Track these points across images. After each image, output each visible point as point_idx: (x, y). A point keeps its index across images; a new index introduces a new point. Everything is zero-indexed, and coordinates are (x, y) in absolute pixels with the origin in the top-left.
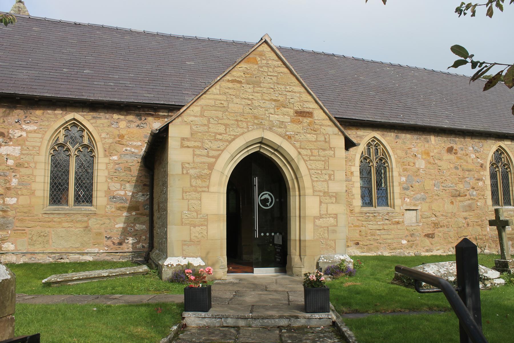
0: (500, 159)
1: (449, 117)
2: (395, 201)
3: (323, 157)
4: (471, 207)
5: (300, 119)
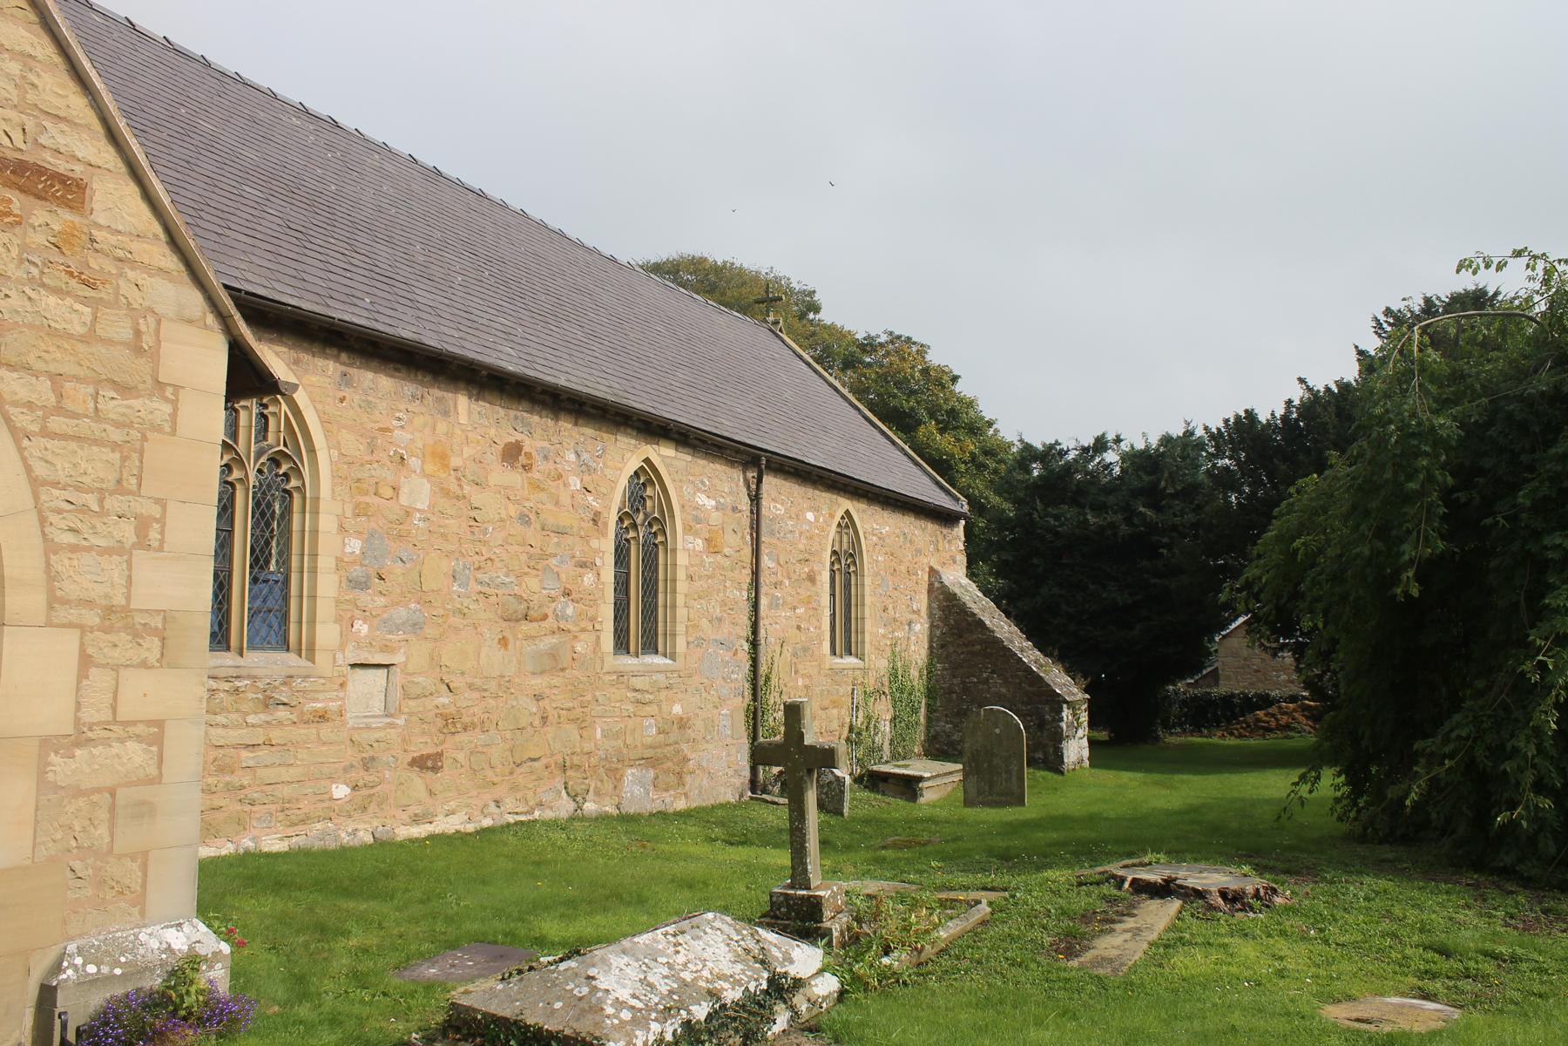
0: (640, 502)
1: (512, 337)
2: (319, 627)
3: (118, 425)
4: (555, 660)
5: (10, 201)
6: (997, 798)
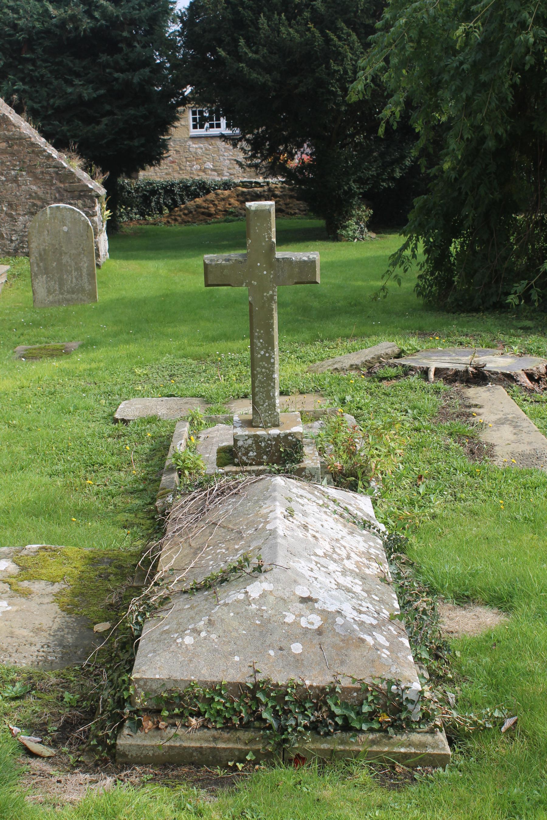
6: (69, 296)
